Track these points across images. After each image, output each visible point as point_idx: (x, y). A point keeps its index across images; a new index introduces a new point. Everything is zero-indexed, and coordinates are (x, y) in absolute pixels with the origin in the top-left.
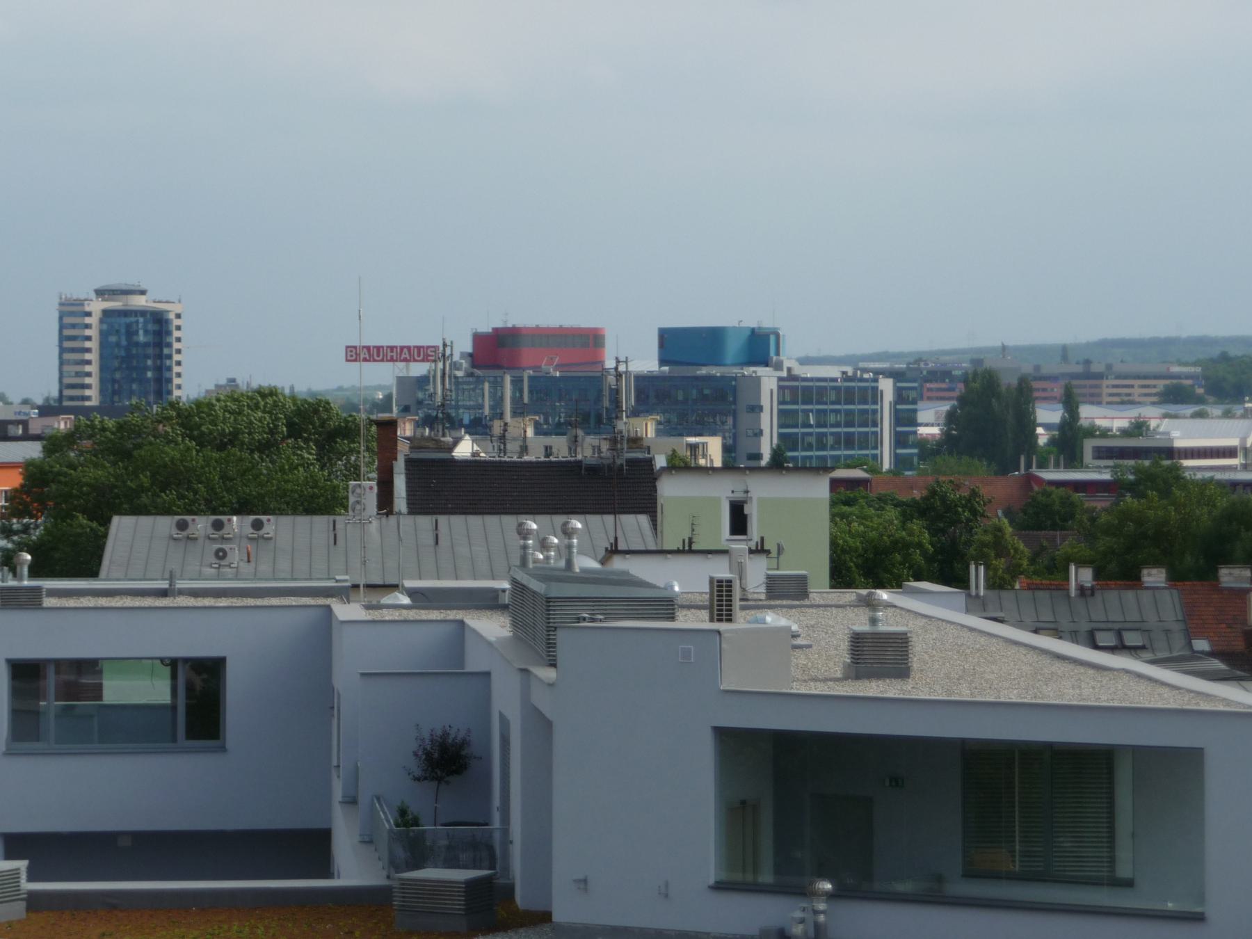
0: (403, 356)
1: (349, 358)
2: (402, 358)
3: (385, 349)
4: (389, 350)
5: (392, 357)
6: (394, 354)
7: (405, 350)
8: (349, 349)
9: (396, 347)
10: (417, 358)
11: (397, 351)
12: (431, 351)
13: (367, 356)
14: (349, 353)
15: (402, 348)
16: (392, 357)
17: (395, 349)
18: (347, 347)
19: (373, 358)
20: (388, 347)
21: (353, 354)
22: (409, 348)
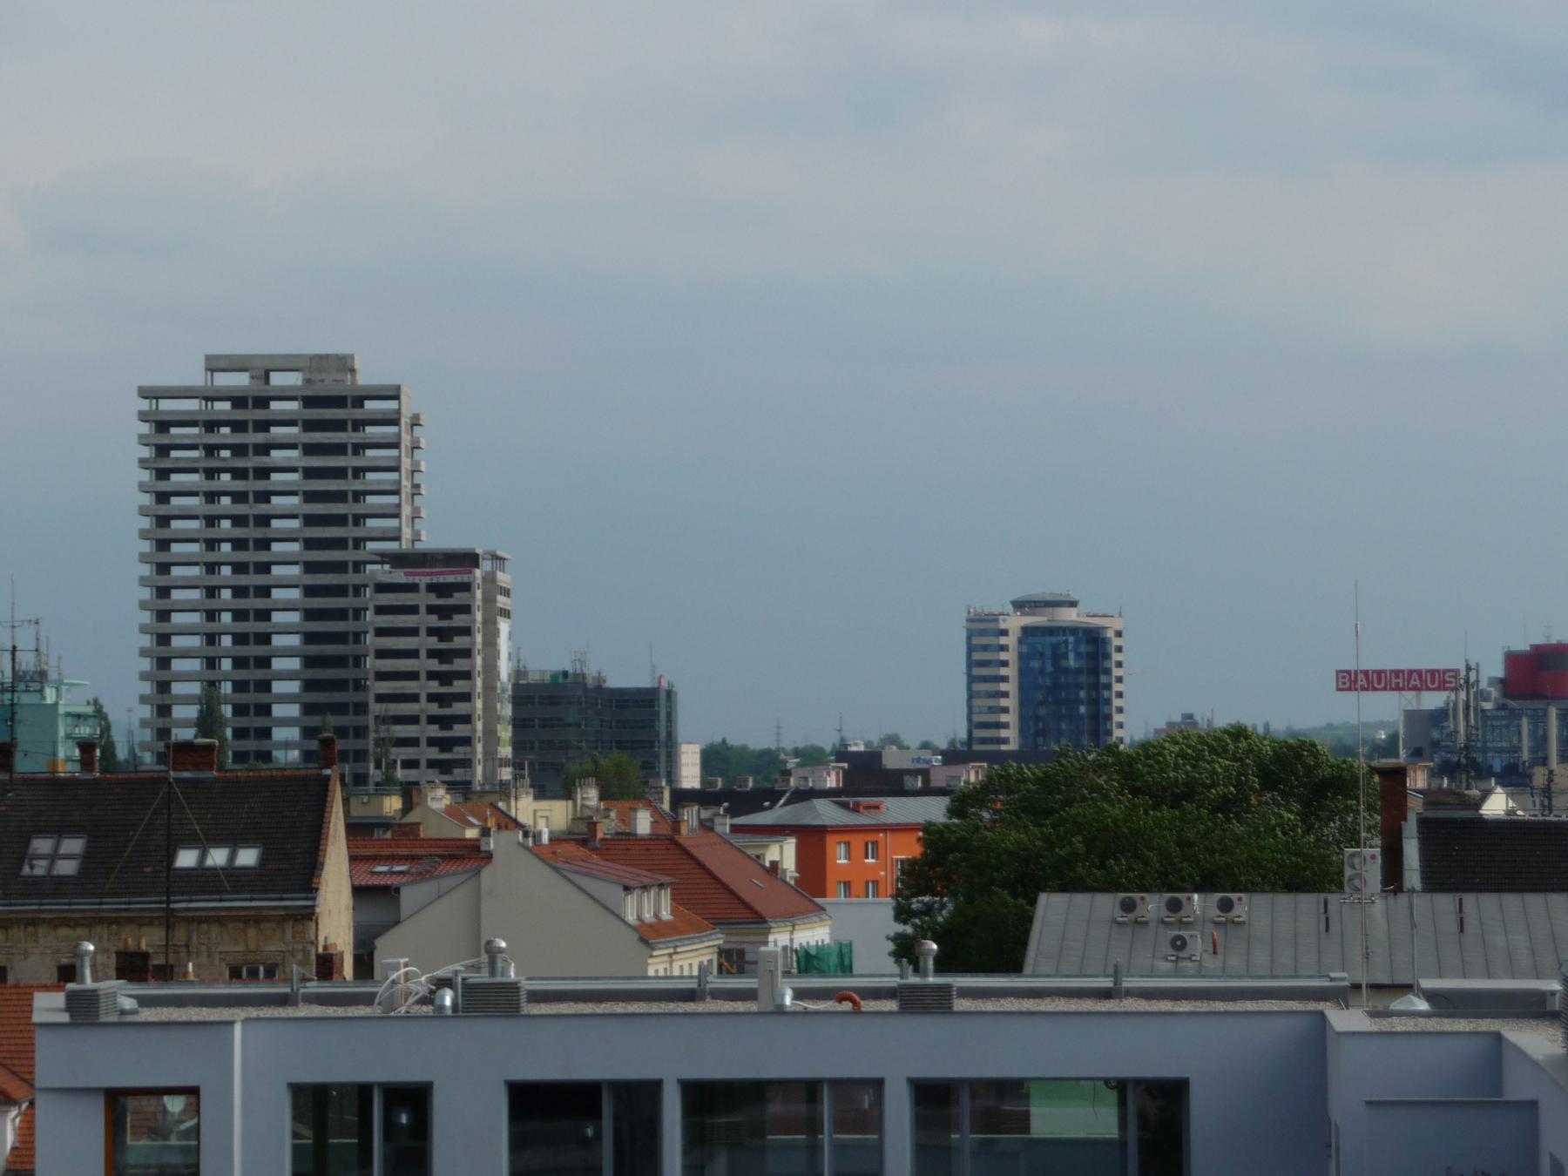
0: (1412, 683)
1: (1341, 686)
2: (1411, 686)
3: (1388, 673)
4: (1401, 685)
5: (1397, 684)
6: (1400, 681)
7: (1415, 675)
8: (1341, 675)
9: (1403, 671)
10: (1376, 686)
11: (1390, 685)
12: (1451, 682)
13: (1418, 683)
14: (1340, 680)
15: (1411, 672)
16: (1397, 684)
17: (1401, 675)
18: (1339, 672)
19: (1373, 686)
20: (1392, 671)
21: (1346, 680)
22: (1419, 672)
